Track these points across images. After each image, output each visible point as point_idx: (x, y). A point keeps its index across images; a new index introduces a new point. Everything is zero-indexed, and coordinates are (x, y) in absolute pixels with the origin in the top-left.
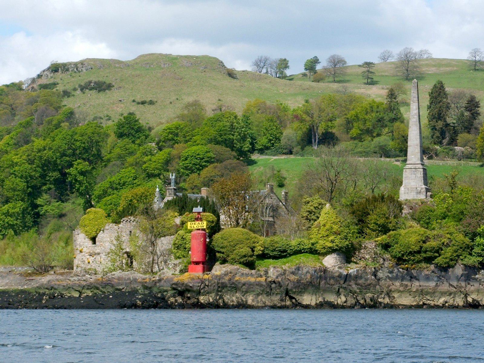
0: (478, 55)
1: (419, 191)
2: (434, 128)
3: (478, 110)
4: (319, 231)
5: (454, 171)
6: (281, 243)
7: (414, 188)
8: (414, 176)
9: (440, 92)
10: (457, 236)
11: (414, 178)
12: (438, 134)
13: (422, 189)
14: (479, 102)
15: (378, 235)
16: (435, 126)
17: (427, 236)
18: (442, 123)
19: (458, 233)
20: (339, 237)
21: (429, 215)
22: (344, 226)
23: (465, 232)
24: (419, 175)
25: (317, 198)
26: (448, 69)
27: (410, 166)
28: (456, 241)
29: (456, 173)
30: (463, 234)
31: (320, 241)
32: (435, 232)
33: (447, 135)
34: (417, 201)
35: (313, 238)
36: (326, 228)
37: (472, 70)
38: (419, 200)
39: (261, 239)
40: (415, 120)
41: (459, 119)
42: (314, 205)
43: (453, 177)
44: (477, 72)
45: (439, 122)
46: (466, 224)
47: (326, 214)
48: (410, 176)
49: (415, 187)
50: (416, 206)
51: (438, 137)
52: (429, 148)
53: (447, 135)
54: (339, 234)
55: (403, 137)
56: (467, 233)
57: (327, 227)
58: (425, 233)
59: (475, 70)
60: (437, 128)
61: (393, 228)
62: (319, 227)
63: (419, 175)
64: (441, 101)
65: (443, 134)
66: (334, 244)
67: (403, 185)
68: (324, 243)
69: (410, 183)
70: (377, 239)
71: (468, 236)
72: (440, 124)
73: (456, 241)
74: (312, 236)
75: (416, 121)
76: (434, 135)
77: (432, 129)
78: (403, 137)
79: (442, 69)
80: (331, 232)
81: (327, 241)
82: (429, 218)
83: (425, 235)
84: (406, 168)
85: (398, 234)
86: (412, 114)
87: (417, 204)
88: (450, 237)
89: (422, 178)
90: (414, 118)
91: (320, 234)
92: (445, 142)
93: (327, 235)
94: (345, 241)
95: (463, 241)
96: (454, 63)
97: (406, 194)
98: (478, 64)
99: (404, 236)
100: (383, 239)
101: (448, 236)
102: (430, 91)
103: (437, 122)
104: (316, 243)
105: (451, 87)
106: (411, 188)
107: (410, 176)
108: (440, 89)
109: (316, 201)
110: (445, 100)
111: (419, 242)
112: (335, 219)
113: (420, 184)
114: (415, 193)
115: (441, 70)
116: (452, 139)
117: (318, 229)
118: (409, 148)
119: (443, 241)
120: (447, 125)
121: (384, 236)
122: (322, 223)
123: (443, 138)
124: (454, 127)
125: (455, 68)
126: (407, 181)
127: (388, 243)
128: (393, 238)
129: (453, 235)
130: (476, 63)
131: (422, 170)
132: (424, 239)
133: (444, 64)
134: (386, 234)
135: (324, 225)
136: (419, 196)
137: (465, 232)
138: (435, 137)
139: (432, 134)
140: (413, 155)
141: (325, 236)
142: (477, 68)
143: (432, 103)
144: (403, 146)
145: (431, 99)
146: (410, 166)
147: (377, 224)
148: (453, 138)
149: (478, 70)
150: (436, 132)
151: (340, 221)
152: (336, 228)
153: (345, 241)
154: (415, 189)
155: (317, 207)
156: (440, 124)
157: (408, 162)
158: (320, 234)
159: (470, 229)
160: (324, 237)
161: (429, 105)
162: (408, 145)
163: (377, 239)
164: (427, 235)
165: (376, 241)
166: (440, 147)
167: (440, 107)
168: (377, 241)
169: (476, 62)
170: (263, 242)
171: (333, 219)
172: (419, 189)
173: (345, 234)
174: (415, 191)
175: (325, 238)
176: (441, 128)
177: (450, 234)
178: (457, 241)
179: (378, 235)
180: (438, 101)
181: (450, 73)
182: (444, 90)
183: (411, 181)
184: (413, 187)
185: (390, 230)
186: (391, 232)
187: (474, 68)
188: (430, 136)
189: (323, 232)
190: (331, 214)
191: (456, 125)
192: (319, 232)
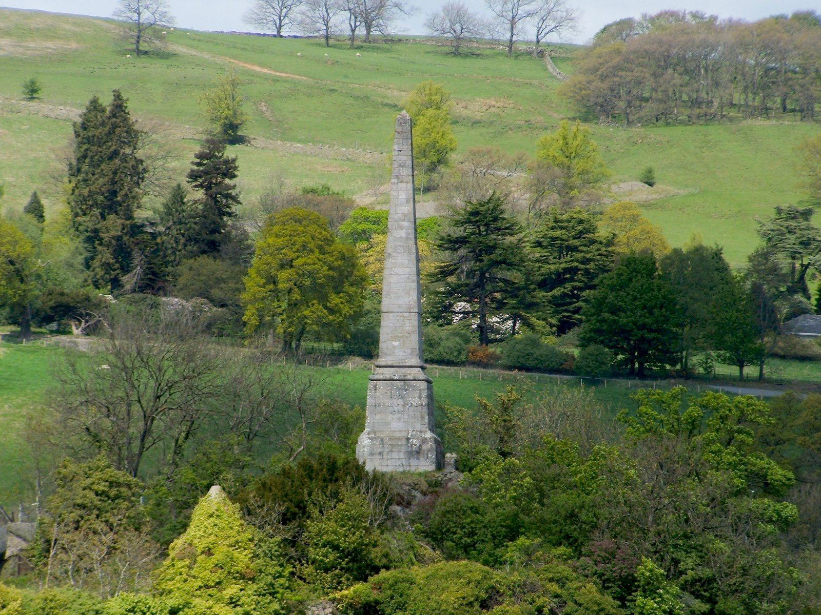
0: (147, 7)
1: (414, 448)
2: (93, 238)
3: (234, 187)
4: (190, 568)
5: (509, 388)
6: (76, 605)
7: (399, 439)
8: (401, 402)
9: (115, 126)
10: (579, 588)
11: (401, 408)
12: (106, 255)
13: (424, 441)
14: (234, 160)
15: (339, 583)
16: (96, 231)
17: (493, 587)
18: (119, 221)
19: (582, 578)
20: (252, 588)
21: (472, 522)
22: (266, 555)
23: (601, 576)
24: (416, 401)
25: (102, 464)
26: (50, 44)
27: (388, 373)
28: (576, 602)
29: (514, 395)
30: (595, 583)
31: (196, 601)
32: (516, 577)
33: (136, 262)
34: (415, 478)
35: (170, 592)
36: (214, 559)
37: (130, 51)
38: (420, 474)
39: (12, 595)
40: (403, 233)
41: (169, 213)
42: (95, 487)
43: (505, 408)
44: (144, 60)
45: (112, 217)
46: (603, 554)
47: (211, 516)
48: (387, 402)
49: (404, 434)
50: (415, 493)
51: (107, 267)
52: (88, 299)
53: (138, 259)
54: (253, 580)
55: (12, 263)
56: (608, 580)
57: (218, 557)
58: (485, 577)
59: (139, 52)
60: (105, 236)
61: (384, 561)
62: (190, 554)
63: (416, 401)
64: (116, 153)
65: (122, 254)
66: (238, 608)
67: (367, 430)
68: (210, 608)
69: (387, 424)
70: (338, 595)
71: (608, 588)
72: (114, 225)
73: (576, 602)
74: (170, 585)
75: (407, 238)
76: (92, 258)
77: (89, 240)
78: (12, 263)
79: (35, 45)
80: (229, 573)
81: (218, 600)
82: (472, 534)
83: (486, 584)
84: (377, 377)
85: (404, 580)
86: (396, 217)
87: (415, 486)
88: (559, 591)
89: (425, 410)
90: (401, 228)
91: (194, 577)
92: (129, 281)
93: (219, 583)
94: (271, 602)
95: (599, 605)
96: (67, 27)
97: (378, 457)
98: (148, 34)
99: (425, 585)
100: (357, 594)
101: (554, 587)
102: (79, 120)
103: (103, 218)
104: (184, 606)
105: (72, 105)
106: (391, 439)
107: (387, 402)
108: (114, 116)
109: (98, 475)
110: (128, 151)
111: (470, 604)
112: (238, 532)
113: (418, 426)
114: (402, 455)
115: (28, 48)
116: (154, 274)
117: (187, 562)
118: (384, 316)
119: (539, 602)
120: (136, 229)
121: (359, 586)
122: (201, 545)
123: (126, 269)
124: (154, 236)
125: (74, 45)
126: (378, 417)
127: (377, 602)
128: (389, 592)
129: (569, 584)
130: (140, 31)
131: (424, 385)
132: (483, 595)
133: (38, 30)
134: (366, 580)
135: (209, 552)
136: (414, 462)
137: (601, 576)
138: (96, 263)
139: (87, 255)
140: (395, 338)
141: (211, 583)
142: (143, 46)
143: (85, 157)
144: (10, 292)
145: (80, 144)
146: (388, 373)
147: (336, 548)
148: (156, 269)
149: (146, 53)
150: (100, 248)
151: (251, 540)
152: (242, 558)
153: (271, 602)
154: (404, 442)
155: (103, 492)
156: (114, 225)
157: (382, 361)
158: (194, 577)
159: (615, 569)
160: (207, 587)
161: (74, 162)
162: (384, 309)
163: (338, 595)
164: (492, 582)
165: (334, 600)
166: (116, 297)
167: (115, 173)
168: (340, 601)
169: (140, 27)
170: (21, 605)
171: (234, 533)
172: (416, 442)
173: (269, 579)
174: (404, 449)
175: (210, 591)
176: (118, 239)
177: (558, 581)
178: (580, 605)
179: (339, 583)
180: (108, 152)
181: (62, 58)
182: (126, 119)
183: (390, 417)
184: (398, 435)
185: (377, 570)
186: (383, 574)
187: (134, 47)
188: (80, 259)
189: (204, 571)
190: (225, 516)
191: (161, 229)
192: (193, 572)
